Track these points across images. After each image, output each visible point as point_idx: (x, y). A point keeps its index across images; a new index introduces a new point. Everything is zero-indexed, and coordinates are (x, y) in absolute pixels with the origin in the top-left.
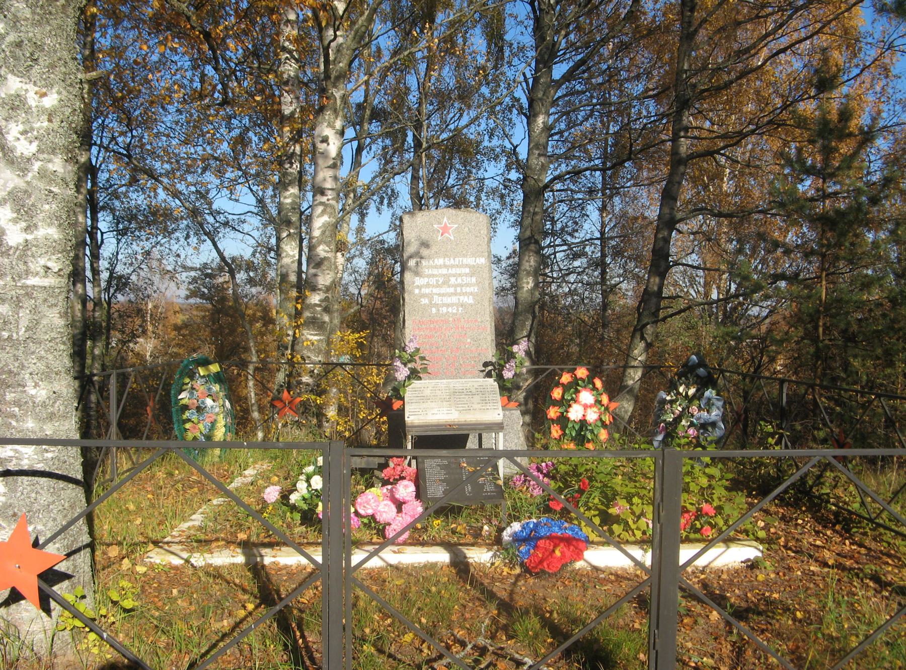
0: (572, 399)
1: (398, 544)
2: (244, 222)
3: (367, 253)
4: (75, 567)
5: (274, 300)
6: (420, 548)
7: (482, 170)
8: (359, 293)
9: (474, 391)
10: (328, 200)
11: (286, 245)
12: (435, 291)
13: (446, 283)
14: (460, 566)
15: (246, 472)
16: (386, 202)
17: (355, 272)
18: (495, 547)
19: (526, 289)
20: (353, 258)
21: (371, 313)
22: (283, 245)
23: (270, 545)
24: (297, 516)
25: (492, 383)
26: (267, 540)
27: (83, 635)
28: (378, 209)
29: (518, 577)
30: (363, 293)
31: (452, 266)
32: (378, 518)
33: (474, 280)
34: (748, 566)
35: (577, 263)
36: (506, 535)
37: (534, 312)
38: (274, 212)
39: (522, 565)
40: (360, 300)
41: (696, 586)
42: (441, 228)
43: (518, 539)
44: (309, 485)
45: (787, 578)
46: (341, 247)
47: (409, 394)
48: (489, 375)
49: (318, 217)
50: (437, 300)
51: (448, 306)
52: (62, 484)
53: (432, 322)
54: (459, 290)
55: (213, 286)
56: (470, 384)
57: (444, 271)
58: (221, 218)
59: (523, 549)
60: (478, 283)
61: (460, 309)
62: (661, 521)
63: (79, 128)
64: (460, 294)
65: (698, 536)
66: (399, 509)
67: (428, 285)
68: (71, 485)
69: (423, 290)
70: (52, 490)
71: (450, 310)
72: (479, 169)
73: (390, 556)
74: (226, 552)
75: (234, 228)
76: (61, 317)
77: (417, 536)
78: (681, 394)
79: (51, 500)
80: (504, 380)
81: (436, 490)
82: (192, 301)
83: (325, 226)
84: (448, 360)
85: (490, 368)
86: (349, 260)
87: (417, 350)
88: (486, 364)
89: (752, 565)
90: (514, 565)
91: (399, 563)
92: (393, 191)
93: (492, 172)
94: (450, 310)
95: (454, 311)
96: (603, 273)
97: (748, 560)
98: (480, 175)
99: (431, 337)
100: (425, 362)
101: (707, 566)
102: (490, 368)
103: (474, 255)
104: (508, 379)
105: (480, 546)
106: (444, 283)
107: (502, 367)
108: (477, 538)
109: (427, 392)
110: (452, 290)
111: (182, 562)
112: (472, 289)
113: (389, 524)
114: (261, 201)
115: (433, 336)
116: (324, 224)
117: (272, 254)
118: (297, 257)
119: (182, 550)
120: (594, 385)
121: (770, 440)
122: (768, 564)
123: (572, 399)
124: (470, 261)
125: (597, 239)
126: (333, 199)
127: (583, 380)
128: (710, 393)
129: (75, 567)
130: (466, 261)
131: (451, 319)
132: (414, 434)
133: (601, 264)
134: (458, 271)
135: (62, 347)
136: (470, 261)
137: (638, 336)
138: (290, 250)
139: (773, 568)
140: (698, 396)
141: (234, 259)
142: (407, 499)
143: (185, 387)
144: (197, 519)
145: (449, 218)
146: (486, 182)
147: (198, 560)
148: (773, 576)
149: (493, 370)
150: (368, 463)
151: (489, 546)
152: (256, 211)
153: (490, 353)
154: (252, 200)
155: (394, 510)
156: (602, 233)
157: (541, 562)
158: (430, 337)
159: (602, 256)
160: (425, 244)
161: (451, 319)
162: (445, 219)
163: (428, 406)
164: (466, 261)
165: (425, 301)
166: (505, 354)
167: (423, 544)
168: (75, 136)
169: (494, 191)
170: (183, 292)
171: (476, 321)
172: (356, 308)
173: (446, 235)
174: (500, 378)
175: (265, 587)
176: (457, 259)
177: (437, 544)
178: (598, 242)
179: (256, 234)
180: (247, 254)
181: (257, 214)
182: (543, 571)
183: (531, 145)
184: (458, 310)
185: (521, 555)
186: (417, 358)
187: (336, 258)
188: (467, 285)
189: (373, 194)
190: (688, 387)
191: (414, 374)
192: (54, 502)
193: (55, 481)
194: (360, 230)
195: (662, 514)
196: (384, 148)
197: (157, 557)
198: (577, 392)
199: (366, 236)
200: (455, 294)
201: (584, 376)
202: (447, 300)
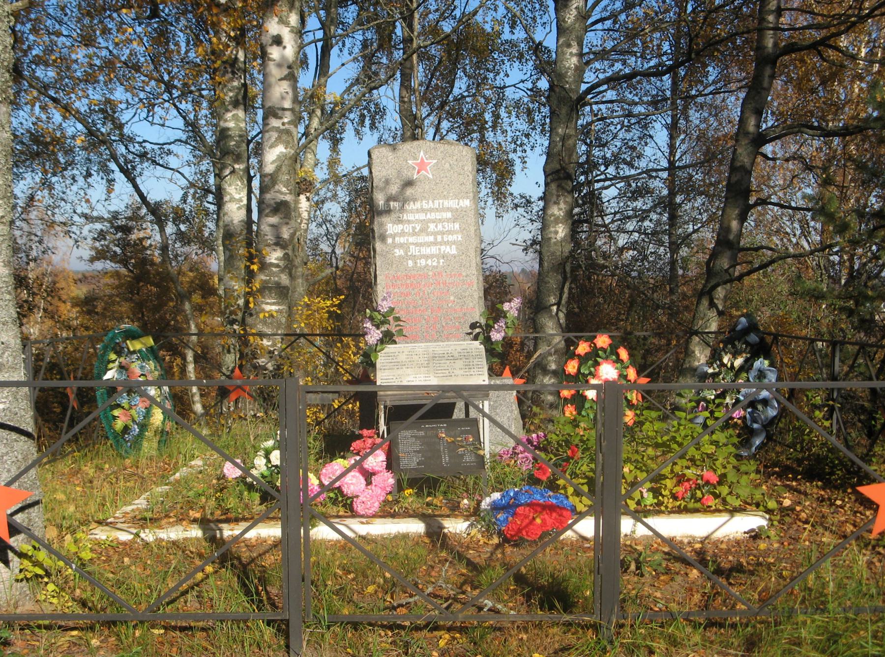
0: (591, 373)
1: (367, 512)
2: (169, 153)
3: (343, 195)
4: (30, 520)
5: (214, 264)
6: (391, 519)
7: (502, 75)
8: (333, 252)
9: (456, 355)
10: (283, 124)
11: (230, 185)
12: (412, 240)
13: (424, 230)
14: (435, 534)
15: (193, 463)
16: (367, 122)
17: (325, 221)
18: (473, 518)
19: (553, 240)
20: (323, 202)
21: (351, 280)
22: (226, 186)
23: (227, 521)
24: (257, 496)
25: (478, 347)
26: (223, 517)
27: (42, 586)
28: (357, 132)
29: (498, 546)
30: (339, 251)
31: (431, 210)
32: (345, 490)
33: (457, 226)
34: (750, 537)
35: (639, 204)
36: (485, 503)
37: (565, 272)
38: (210, 138)
39: (500, 533)
40: (334, 260)
41: (689, 554)
42: (417, 164)
43: (496, 507)
44: (269, 461)
45: (791, 547)
46: (304, 186)
47: (381, 360)
48: (476, 338)
49: (271, 147)
50: (413, 250)
51: (427, 257)
52: (14, 436)
53: (408, 277)
54: (439, 238)
55: (129, 244)
56: (452, 347)
57: (422, 216)
58: (136, 148)
59: (501, 516)
60: (462, 230)
61: (441, 261)
62: (603, 450)
63: (11, 66)
64: (441, 244)
65: (698, 505)
66: (369, 483)
67: (403, 234)
68: (23, 438)
69: (397, 239)
70: (5, 441)
71: (429, 262)
72: (498, 73)
73: (358, 528)
74: (180, 528)
75: (155, 163)
76: (5, 266)
77: (387, 511)
78: (726, 365)
79: (4, 451)
80: (492, 343)
81: (410, 460)
82: (99, 265)
83: (281, 158)
84: (427, 322)
85: (478, 330)
86: (319, 204)
87: (392, 310)
88: (473, 326)
89: (755, 535)
90: (491, 535)
91: (368, 534)
92: (377, 105)
93: (516, 78)
94: (429, 262)
95: (435, 264)
96: (673, 218)
97: (752, 530)
98: (498, 83)
99: (408, 294)
100: (401, 323)
101: (707, 538)
102: (478, 330)
103: (456, 197)
104: (496, 341)
105: (456, 516)
106: (421, 231)
107: (489, 328)
108: (454, 510)
109: (402, 358)
110: (431, 239)
111: (132, 536)
112: (455, 237)
113: (357, 497)
114: (192, 126)
115: (410, 294)
116: (279, 157)
117: (210, 198)
118: (245, 202)
119: (130, 527)
120: (618, 355)
121: (817, 413)
122: (772, 533)
123: (591, 373)
124: (452, 203)
125: (665, 169)
126: (289, 123)
127: (604, 350)
128: (761, 363)
129: (30, 520)
130: (447, 203)
131: (431, 273)
132: (389, 403)
133: (669, 205)
134: (438, 216)
135: (8, 297)
136: (452, 203)
137: (705, 302)
138: (236, 193)
139: (778, 538)
140: (746, 367)
141: (158, 205)
142: (377, 468)
143: (111, 365)
144: (141, 503)
145: (426, 153)
146: (509, 92)
147: (148, 536)
148: (776, 545)
149: (480, 332)
150: (322, 399)
151: (467, 518)
152: (184, 137)
153: (476, 311)
154: (180, 123)
155: (363, 482)
156: (671, 163)
157: (520, 530)
158: (408, 294)
159: (669, 194)
160: (409, 183)
161: (431, 273)
162: (422, 153)
163: (403, 369)
164: (447, 203)
165: (398, 252)
166: (495, 313)
167: (393, 516)
168: (7, 75)
169: (517, 104)
170: (87, 253)
171: (460, 275)
172: (329, 271)
173: (423, 172)
174: (487, 341)
175: (226, 556)
176: (436, 202)
177: (410, 516)
178: (665, 175)
179: (186, 171)
180: (176, 197)
181: (186, 143)
182: (522, 539)
183: (560, 43)
184: (438, 262)
185: (498, 523)
186: (391, 318)
187: (297, 202)
188: (450, 232)
189: (350, 111)
190: (735, 355)
191: (388, 338)
192: (7, 453)
193: (8, 432)
194: (333, 163)
195: (603, 444)
196: (365, 44)
197: (102, 534)
198: (597, 364)
199: (342, 170)
200: (435, 243)
201: (605, 345)
202: (426, 251)
